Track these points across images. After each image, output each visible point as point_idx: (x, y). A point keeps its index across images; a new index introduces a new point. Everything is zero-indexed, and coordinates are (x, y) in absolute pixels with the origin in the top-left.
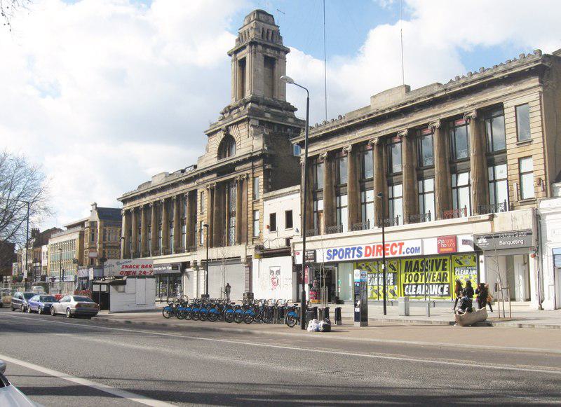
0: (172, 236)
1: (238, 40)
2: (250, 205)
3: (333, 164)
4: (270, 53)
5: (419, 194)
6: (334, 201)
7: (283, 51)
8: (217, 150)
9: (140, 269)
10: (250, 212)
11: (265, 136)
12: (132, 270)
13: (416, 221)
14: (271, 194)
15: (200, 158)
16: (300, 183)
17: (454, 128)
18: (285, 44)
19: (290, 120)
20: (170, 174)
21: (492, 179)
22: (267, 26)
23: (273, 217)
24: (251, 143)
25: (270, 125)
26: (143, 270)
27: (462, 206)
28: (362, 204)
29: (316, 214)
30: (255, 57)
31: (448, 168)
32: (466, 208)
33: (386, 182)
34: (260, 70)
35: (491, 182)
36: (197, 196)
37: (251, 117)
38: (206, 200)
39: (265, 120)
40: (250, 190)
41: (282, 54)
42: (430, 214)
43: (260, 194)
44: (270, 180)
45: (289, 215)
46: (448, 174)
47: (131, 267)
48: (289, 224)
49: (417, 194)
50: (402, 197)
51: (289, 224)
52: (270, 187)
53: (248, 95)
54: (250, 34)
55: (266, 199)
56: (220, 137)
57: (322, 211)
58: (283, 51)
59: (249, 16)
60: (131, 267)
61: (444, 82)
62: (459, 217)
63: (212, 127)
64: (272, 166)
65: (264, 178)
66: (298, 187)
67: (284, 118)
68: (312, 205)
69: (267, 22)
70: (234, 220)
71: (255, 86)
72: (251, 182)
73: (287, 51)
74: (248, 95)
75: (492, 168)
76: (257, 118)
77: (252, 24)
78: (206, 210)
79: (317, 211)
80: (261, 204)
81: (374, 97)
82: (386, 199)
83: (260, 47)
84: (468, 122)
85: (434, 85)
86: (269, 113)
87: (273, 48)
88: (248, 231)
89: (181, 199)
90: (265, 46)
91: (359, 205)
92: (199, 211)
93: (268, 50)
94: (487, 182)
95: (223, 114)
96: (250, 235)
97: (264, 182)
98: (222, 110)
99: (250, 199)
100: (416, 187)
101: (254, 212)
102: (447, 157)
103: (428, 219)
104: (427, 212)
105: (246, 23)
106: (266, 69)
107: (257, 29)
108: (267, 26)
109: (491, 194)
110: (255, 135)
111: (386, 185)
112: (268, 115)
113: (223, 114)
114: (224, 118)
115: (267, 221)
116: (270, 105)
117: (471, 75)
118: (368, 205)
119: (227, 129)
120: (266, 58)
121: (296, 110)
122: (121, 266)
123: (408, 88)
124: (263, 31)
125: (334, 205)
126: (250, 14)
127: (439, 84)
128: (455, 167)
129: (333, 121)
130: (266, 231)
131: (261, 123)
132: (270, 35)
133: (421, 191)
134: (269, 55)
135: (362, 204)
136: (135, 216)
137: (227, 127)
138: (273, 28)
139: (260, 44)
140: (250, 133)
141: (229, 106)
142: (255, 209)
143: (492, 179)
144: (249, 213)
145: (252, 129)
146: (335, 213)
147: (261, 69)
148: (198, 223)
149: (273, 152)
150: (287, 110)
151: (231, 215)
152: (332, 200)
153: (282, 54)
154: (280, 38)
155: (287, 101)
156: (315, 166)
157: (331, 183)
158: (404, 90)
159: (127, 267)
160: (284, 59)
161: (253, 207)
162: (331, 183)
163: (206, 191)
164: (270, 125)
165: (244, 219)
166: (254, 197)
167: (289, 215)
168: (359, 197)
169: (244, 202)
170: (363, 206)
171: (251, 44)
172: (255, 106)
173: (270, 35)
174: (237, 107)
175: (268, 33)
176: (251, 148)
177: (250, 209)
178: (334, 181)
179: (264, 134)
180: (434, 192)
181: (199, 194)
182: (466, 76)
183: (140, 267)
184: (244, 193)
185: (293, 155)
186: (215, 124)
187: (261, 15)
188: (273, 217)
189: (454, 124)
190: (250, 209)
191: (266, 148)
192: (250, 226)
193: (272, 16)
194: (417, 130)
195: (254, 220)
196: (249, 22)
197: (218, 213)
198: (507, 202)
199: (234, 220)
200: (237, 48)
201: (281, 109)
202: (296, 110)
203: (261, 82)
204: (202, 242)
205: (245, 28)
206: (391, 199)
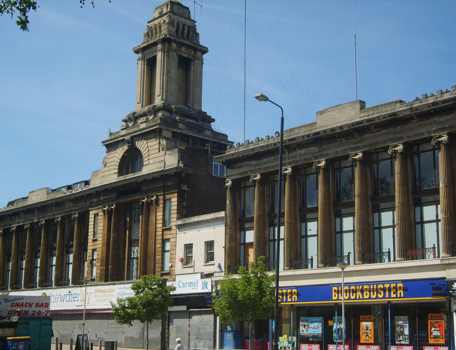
0: (52, 266)
1: (147, 35)
2: (159, 233)
3: (266, 188)
4: (184, 52)
5: (337, 233)
6: (267, 232)
7: (200, 50)
8: (118, 164)
9: (34, 308)
10: (159, 241)
11: (180, 151)
12: (24, 309)
13: (333, 264)
14: (188, 221)
15: (95, 173)
16: (224, 209)
17: (418, 153)
18: (203, 41)
19: (208, 132)
20: (53, 190)
21: (377, 226)
22: (183, 20)
23: (189, 248)
24: (162, 158)
25: (184, 138)
26: (37, 309)
27: (385, 250)
28: (302, 237)
29: (242, 247)
30: (168, 56)
31: (411, 201)
32: (389, 252)
33: (333, 213)
34: (173, 71)
35: (376, 228)
36: (88, 218)
37: (163, 127)
38: (102, 224)
39: (179, 131)
40: (160, 215)
41: (199, 54)
42: (312, 259)
43: (174, 222)
44: (185, 203)
45: (210, 245)
46: (412, 207)
47: (22, 305)
48: (210, 257)
49: (372, 228)
50: (317, 235)
51: (210, 257)
52: (184, 211)
53: (158, 101)
54: (162, 29)
55: (180, 227)
56: (120, 152)
57: (251, 244)
58: (200, 50)
59: (161, 7)
60: (22, 305)
61: (409, 99)
62: (381, 262)
63: (112, 137)
64: (188, 187)
65: (178, 201)
66: (222, 214)
67: (201, 130)
68: (238, 236)
69: (181, 16)
70: (136, 252)
71: (167, 91)
72: (161, 209)
73: (204, 51)
74: (158, 101)
75: (339, 219)
76: (170, 129)
77: (166, 18)
78: (100, 237)
79: (244, 244)
80: (173, 232)
81: (322, 113)
82: (333, 232)
83: (174, 45)
84: (354, 164)
85: (396, 102)
86: (183, 123)
87: (189, 47)
88: (155, 264)
89: (67, 220)
90: (180, 45)
91: (299, 238)
92: (90, 237)
93: (183, 49)
94: (48, 266)
95: (125, 121)
96: (158, 269)
97: (178, 205)
98: (124, 117)
99: (160, 225)
100: (371, 221)
101: (164, 241)
102: (410, 186)
103: (310, 265)
104: (310, 257)
105: (157, 15)
106: (180, 71)
107: (171, 23)
108: (183, 20)
109: (337, 243)
110: (168, 149)
111: (333, 217)
112: (181, 126)
113: (125, 121)
114: (127, 128)
115: (180, 253)
116: (184, 115)
117: (442, 93)
118: (309, 239)
119: (132, 142)
120: (181, 58)
121: (213, 120)
122: (10, 303)
123: (362, 104)
124: (178, 27)
125: (267, 237)
126: (163, 5)
127: (401, 101)
128: (420, 199)
129: (268, 138)
130: (178, 266)
131: (175, 135)
132: (186, 31)
133: (376, 225)
134: (185, 55)
135: (302, 237)
136: (17, 238)
137: (132, 138)
138: (188, 22)
139: (175, 41)
140: (161, 146)
141: (135, 113)
142: (166, 237)
143: (377, 226)
144: (157, 242)
145: (164, 142)
146: (267, 247)
147: (174, 70)
148: (89, 252)
149: (190, 171)
150: (203, 120)
151: (132, 243)
152: (236, 235)
153: (199, 54)
154: (197, 35)
155: (203, 110)
156: (242, 191)
157: (264, 210)
158: (358, 106)
159: (17, 305)
160: (201, 60)
161: (163, 235)
162: (264, 210)
163: (101, 214)
164: (184, 138)
165: (151, 250)
166: (164, 224)
167: (210, 245)
168: (299, 229)
169: (151, 229)
170: (303, 239)
171: (164, 41)
172: (167, 114)
173: (186, 31)
174: (144, 115)
175: (183, 29)
176: (163, 164)
177: (159, 238)
178: (267, 208)
179: (180, 150)
180: (393, 226)
181: (92, 216)
182: (435, 94)
183: (34, 305)
184: (152, 218)
185: (212, 175)
186: (117, 133)
187: (175, 7)
188: (189, 248)
189: (418, 148)
190: (159, 238)
191: (181, 165)
192: (158, 257)
193: (188, 8)
194: (374, 153)
195: (164, 251)
196: (161, 15)
197: (116, 241)
198: (436, 246)
199: (136, 252)
200: (145, 45)
201: (196, 119)
202: (213, 120)
203: (174, 87)
204: (94, 275)
205: (157, 22)
206: (338, 233)
